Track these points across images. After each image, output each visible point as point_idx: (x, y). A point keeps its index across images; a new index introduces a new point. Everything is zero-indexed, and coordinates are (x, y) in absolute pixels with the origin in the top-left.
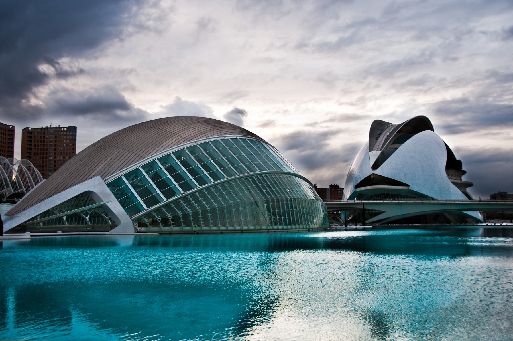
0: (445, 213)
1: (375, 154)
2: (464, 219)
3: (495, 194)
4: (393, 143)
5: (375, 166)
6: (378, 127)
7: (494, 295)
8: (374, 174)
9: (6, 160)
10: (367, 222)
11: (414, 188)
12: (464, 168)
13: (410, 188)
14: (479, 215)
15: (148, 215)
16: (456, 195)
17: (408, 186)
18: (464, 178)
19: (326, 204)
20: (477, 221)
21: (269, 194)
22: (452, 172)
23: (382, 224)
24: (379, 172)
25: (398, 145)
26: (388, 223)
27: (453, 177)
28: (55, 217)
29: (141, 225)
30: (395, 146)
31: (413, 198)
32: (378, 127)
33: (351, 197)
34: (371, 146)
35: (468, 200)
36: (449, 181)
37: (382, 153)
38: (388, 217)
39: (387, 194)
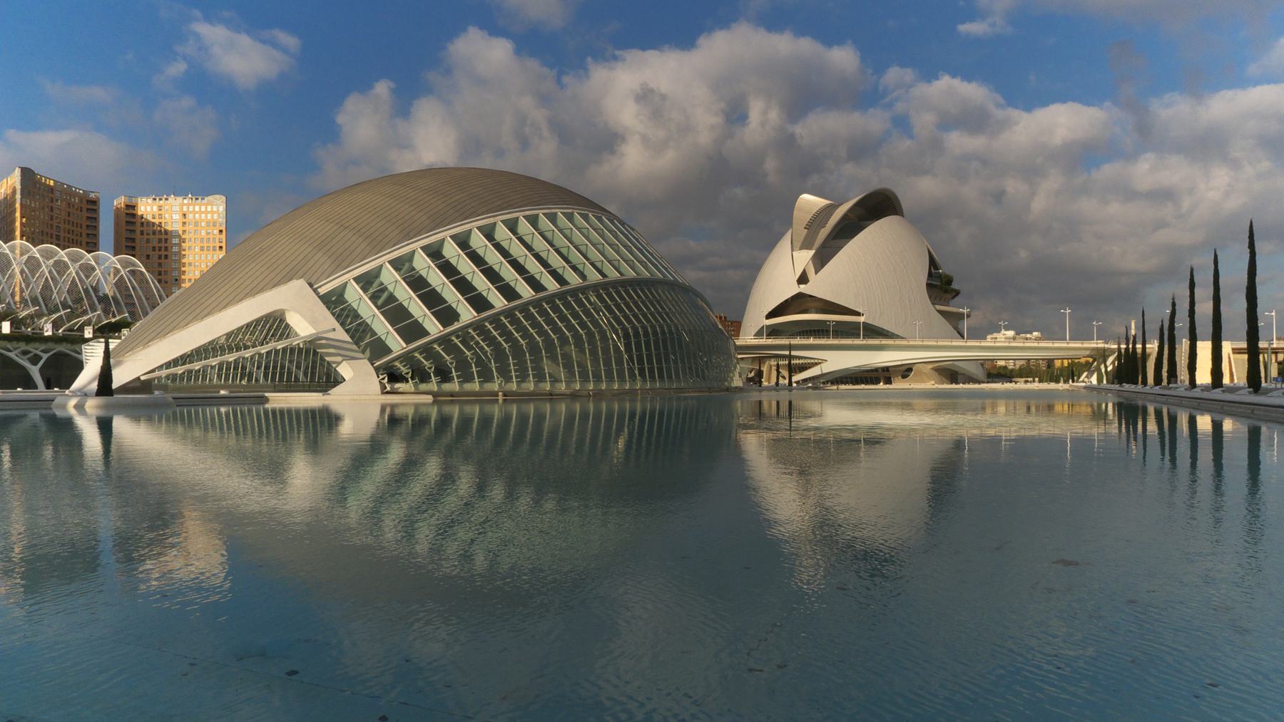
5: (803, 279)
15: (407, 358)
21: (630, 322)
28: (197, 366)
29: (394, 377)
33: (759, 334)
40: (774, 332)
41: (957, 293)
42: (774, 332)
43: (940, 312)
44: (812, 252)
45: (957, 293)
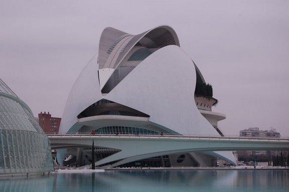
0: (193, 154)
1: (106, 74)
2: (212, 161)
3: (245, 130)
4: (130, 59)
5: (106, 90)
6: (110, 37)
7: (13, 175)
8: (104, 101)
9: (96, 105)
10: (97, 164)
11: (153, 119)
12: (215, 96)
13: (151, 119)
14: (231, 156)
16: (206, 130)
17: (148, 116)
18: (215, 110)
19: (51, 139)
20: (229, 164)
22: (202, 99)
23: (115, 167)
24: (108, 97)
25: (135, 62)
26: (121, 166)
27: (202, 107)
30: (132, 63)
31: (153, 133)
32: (110, 37)
33: (72, 131)
34: (102, 64)
35: (220, 136)
36: (199, 112)
37: (116, 72)
38: (121, 158)
39: (120, 127)
40: (84, 129)
41: (216, 102)
42: (84, 129)
43: (204, 115)
44: (113, 70)
45: (216, 102)
